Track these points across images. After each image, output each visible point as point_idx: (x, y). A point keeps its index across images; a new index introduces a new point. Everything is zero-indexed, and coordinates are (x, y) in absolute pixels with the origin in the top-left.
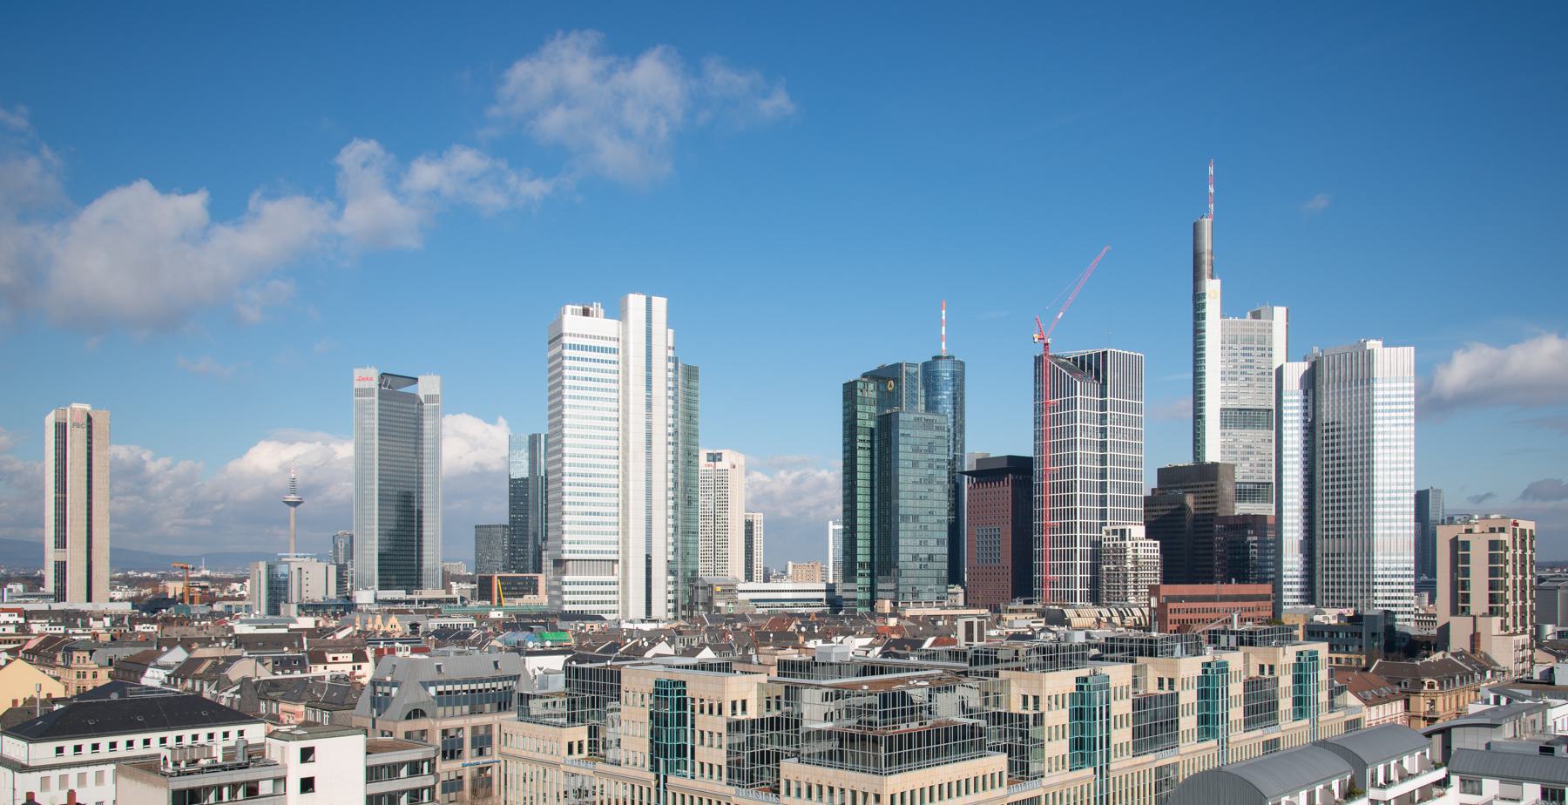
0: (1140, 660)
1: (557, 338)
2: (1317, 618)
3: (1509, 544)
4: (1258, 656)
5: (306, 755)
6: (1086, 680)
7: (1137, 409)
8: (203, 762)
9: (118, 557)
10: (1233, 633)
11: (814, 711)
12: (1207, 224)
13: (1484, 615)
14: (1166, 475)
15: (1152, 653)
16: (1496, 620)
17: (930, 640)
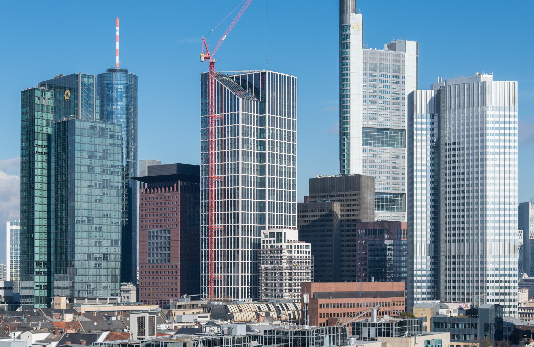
7: (293, 125)
10: (373, 325)
14: (318, 186)
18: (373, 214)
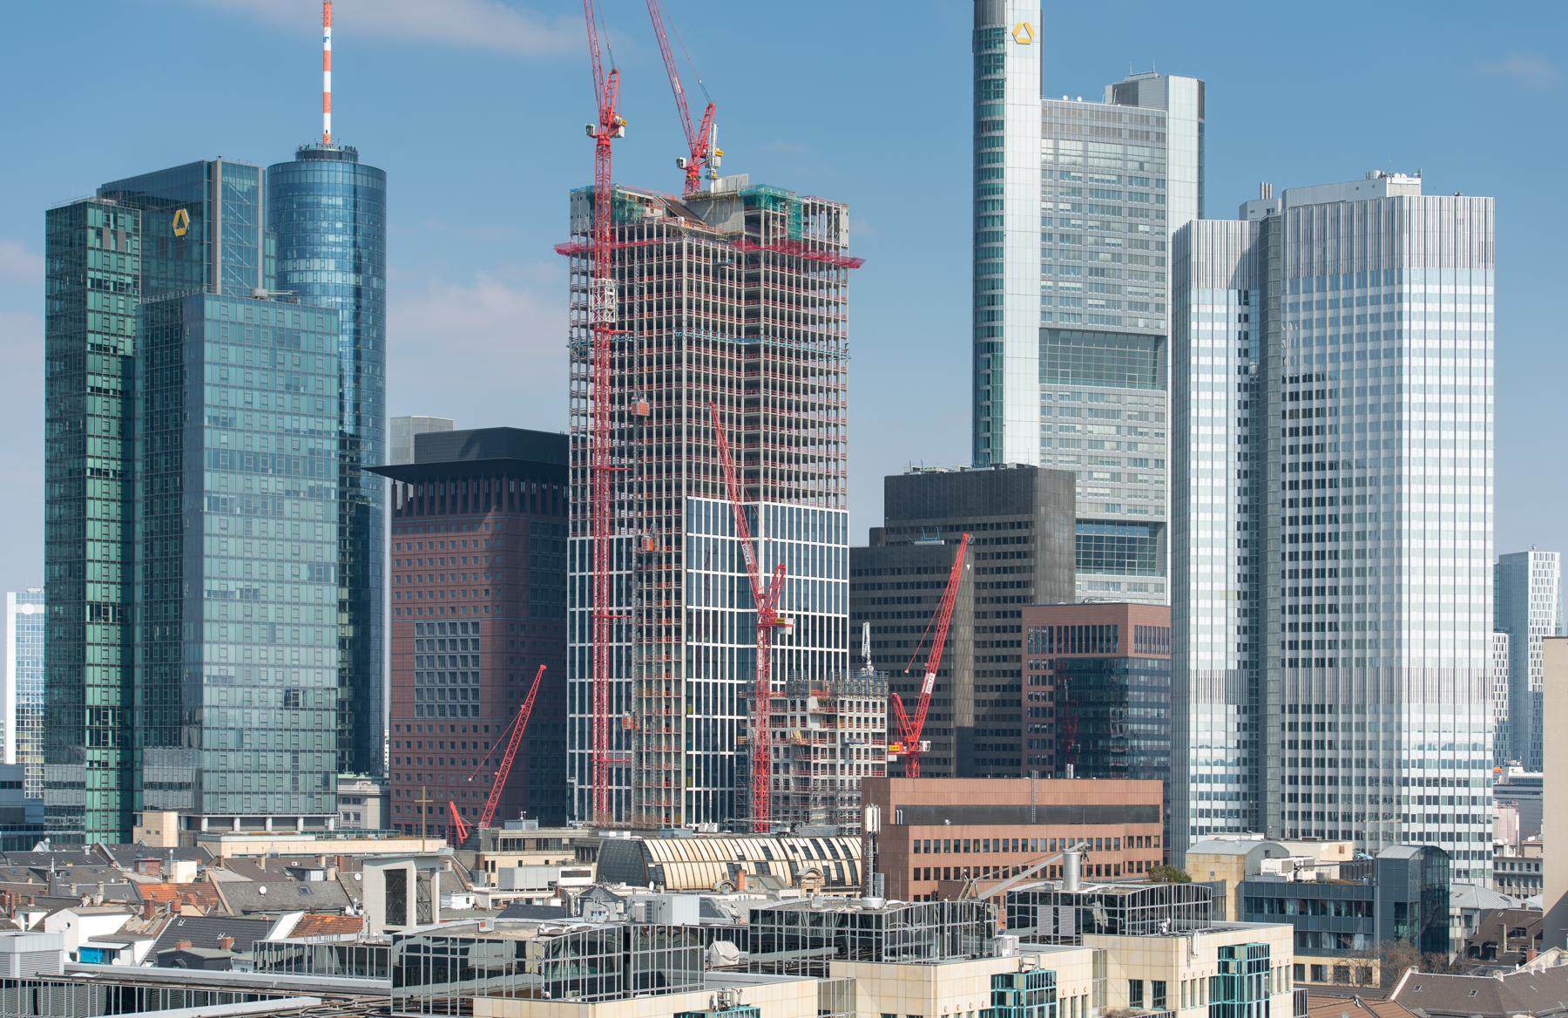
0: (840, 970)
4: (1132, 956)
10: (1068, 899)
14: (910, 497)
15: (869, 951)
17: (288, 922)
18: (1072, 581)
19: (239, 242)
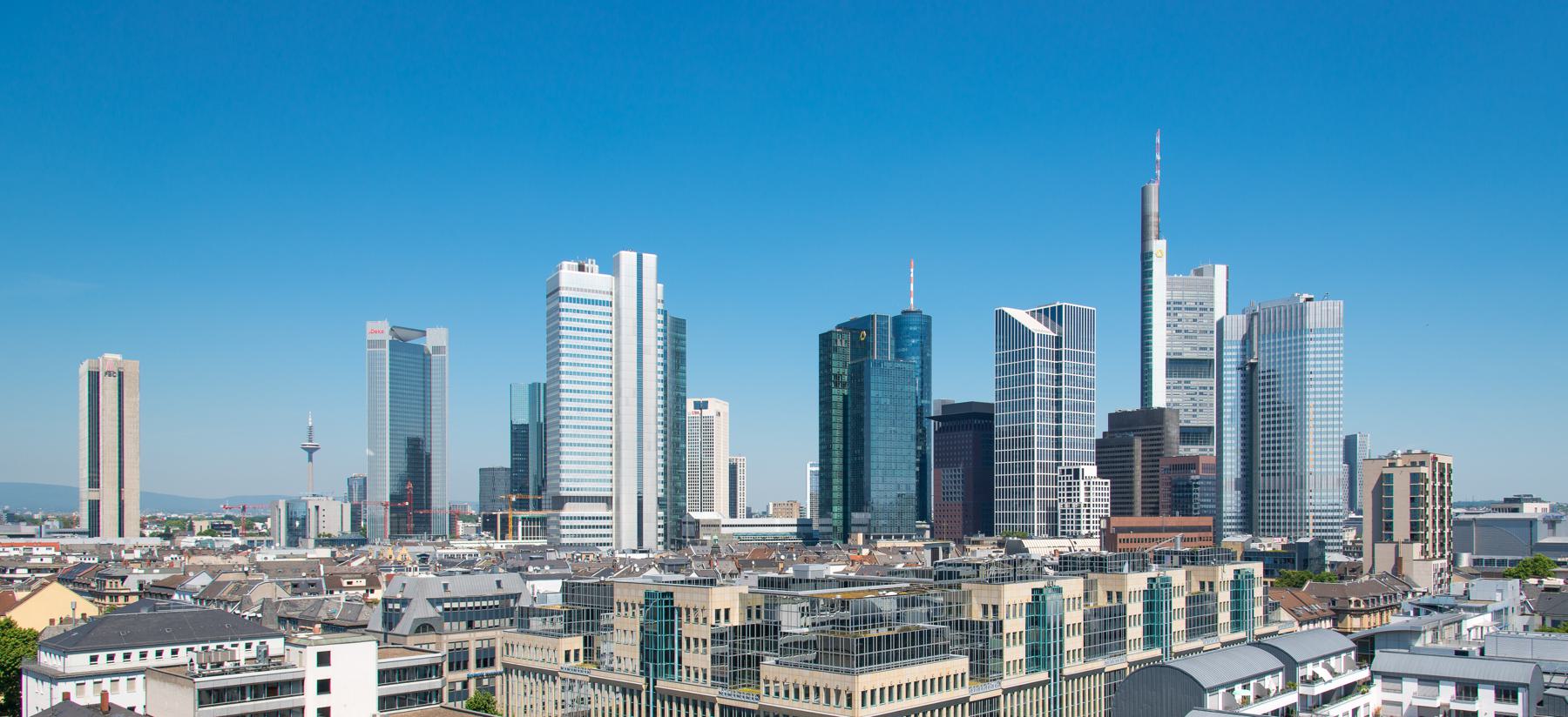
0: (1091, 576)
1: (553, 292)
2: (1254, 545)
3: (1429, 476)
4: (1201, 573)
5: (324, 659)
6: (1040, 591)
8: (227, 665)
9: (146, 499)
11: (792, 621)
12: (1154, 189)
13: (1406, 542)
14: (1117, 420)
16: (1417, 546)
19: (883, 351)
